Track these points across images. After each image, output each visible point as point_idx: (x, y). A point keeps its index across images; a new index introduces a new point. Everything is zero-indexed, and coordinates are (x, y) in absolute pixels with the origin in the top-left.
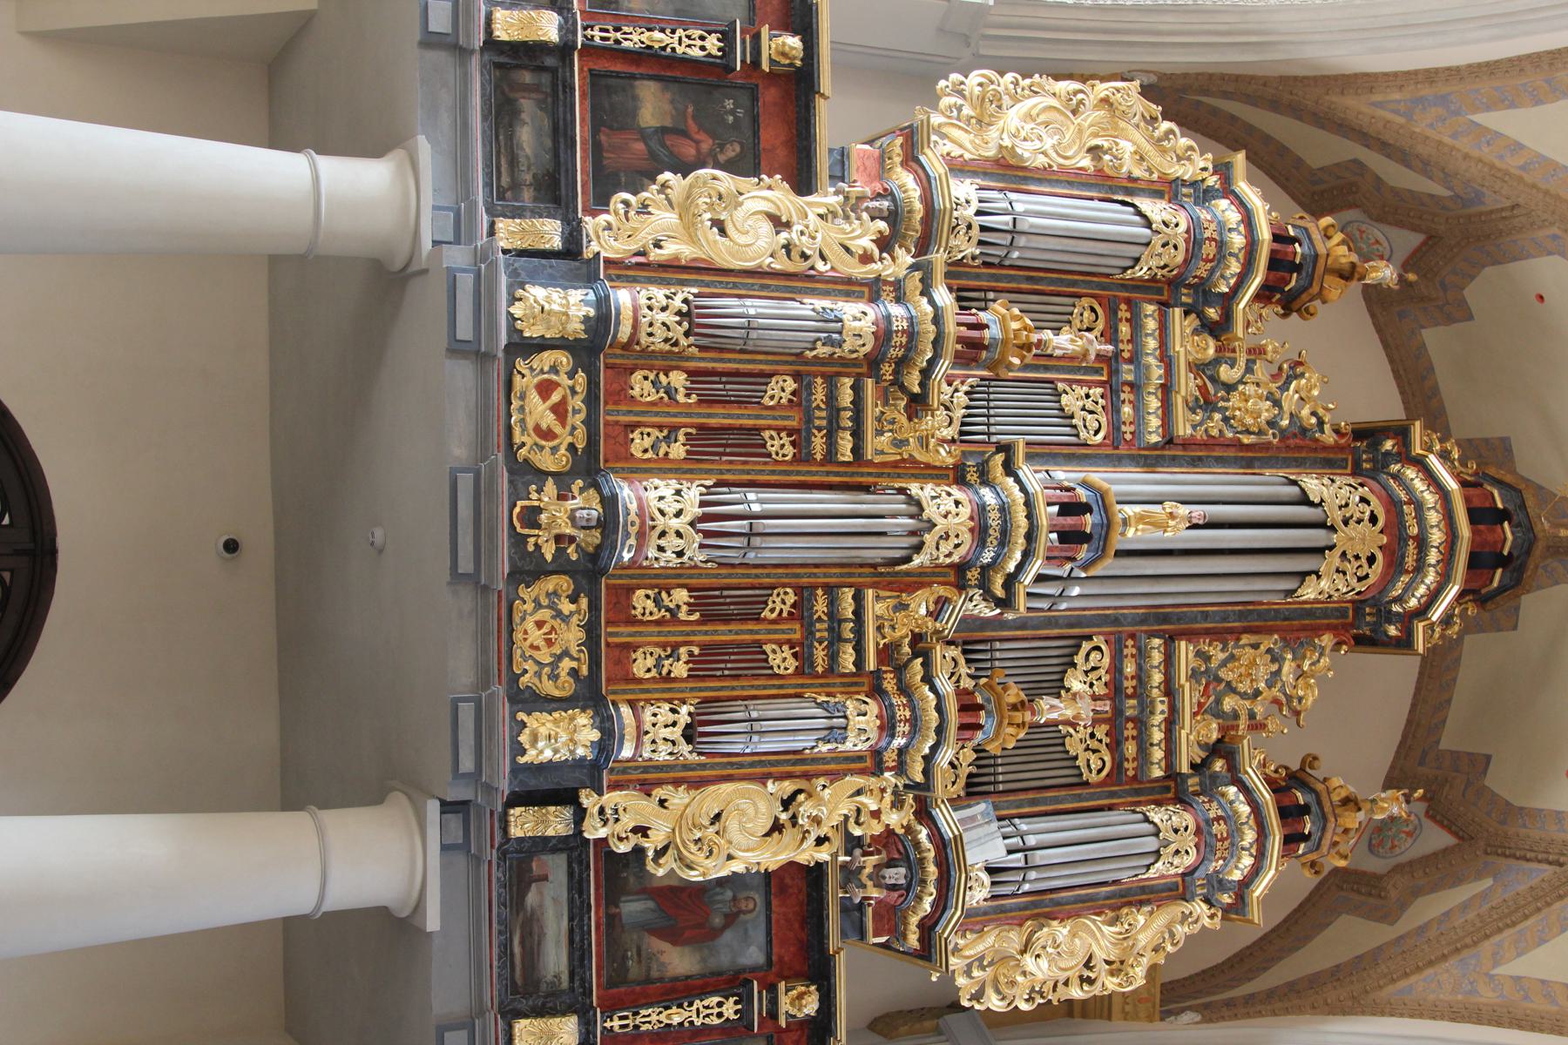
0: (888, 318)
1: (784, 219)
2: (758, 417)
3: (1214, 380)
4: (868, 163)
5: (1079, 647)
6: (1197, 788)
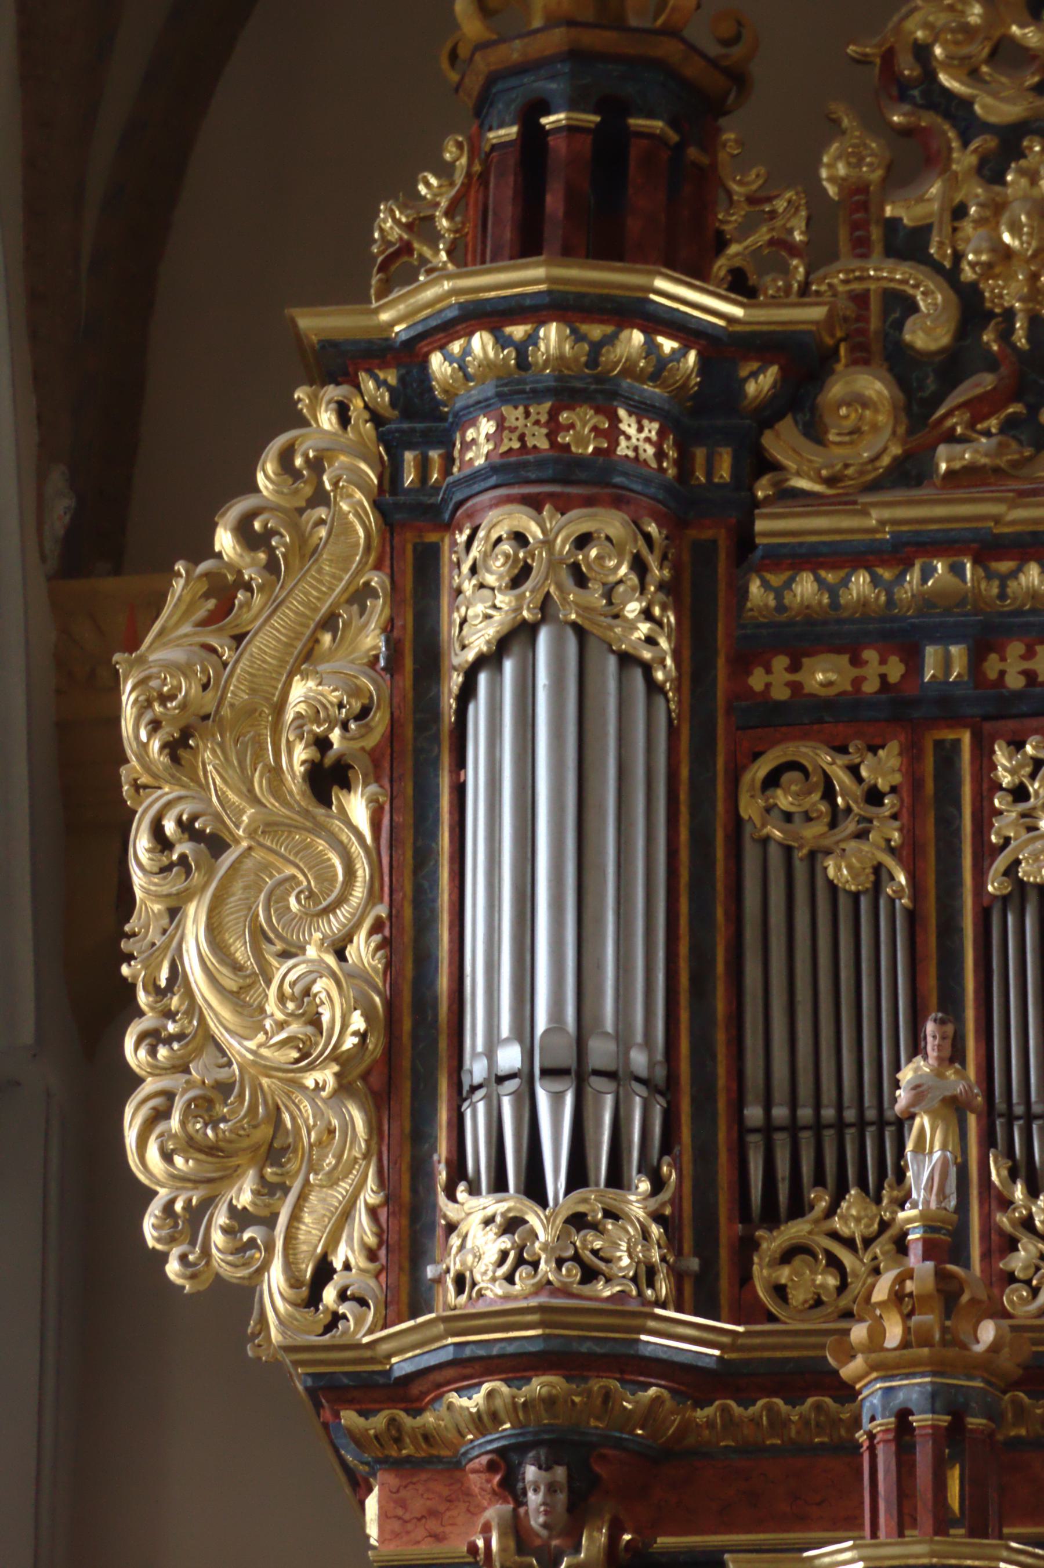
4: (418, 1505)
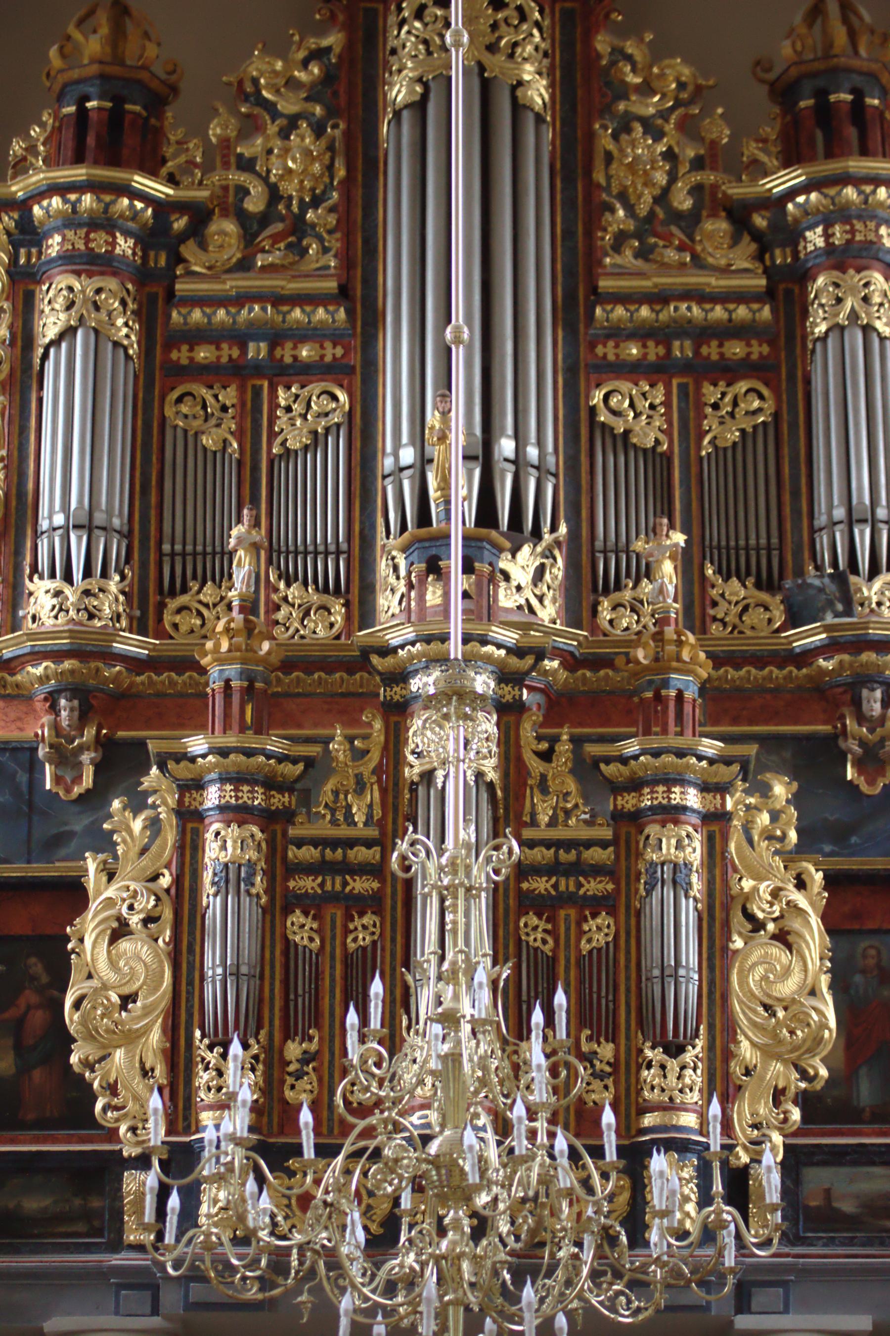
0: (222, 809)
1: (115, 925)
2: (333, 957)
3: (265, 219)
4: (13, 715)
5: (603, 424)
6: (788, 251)
